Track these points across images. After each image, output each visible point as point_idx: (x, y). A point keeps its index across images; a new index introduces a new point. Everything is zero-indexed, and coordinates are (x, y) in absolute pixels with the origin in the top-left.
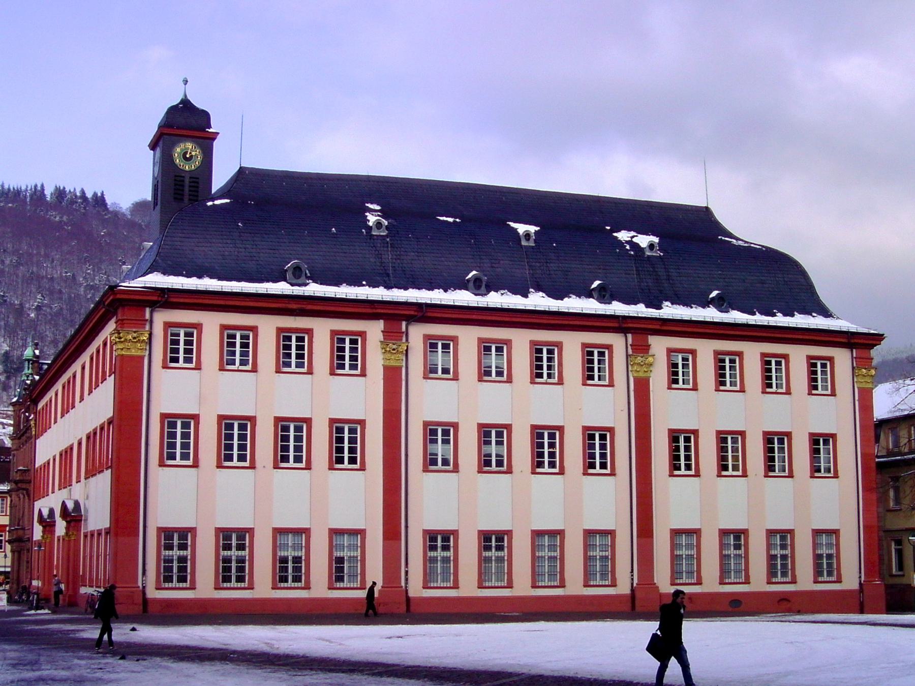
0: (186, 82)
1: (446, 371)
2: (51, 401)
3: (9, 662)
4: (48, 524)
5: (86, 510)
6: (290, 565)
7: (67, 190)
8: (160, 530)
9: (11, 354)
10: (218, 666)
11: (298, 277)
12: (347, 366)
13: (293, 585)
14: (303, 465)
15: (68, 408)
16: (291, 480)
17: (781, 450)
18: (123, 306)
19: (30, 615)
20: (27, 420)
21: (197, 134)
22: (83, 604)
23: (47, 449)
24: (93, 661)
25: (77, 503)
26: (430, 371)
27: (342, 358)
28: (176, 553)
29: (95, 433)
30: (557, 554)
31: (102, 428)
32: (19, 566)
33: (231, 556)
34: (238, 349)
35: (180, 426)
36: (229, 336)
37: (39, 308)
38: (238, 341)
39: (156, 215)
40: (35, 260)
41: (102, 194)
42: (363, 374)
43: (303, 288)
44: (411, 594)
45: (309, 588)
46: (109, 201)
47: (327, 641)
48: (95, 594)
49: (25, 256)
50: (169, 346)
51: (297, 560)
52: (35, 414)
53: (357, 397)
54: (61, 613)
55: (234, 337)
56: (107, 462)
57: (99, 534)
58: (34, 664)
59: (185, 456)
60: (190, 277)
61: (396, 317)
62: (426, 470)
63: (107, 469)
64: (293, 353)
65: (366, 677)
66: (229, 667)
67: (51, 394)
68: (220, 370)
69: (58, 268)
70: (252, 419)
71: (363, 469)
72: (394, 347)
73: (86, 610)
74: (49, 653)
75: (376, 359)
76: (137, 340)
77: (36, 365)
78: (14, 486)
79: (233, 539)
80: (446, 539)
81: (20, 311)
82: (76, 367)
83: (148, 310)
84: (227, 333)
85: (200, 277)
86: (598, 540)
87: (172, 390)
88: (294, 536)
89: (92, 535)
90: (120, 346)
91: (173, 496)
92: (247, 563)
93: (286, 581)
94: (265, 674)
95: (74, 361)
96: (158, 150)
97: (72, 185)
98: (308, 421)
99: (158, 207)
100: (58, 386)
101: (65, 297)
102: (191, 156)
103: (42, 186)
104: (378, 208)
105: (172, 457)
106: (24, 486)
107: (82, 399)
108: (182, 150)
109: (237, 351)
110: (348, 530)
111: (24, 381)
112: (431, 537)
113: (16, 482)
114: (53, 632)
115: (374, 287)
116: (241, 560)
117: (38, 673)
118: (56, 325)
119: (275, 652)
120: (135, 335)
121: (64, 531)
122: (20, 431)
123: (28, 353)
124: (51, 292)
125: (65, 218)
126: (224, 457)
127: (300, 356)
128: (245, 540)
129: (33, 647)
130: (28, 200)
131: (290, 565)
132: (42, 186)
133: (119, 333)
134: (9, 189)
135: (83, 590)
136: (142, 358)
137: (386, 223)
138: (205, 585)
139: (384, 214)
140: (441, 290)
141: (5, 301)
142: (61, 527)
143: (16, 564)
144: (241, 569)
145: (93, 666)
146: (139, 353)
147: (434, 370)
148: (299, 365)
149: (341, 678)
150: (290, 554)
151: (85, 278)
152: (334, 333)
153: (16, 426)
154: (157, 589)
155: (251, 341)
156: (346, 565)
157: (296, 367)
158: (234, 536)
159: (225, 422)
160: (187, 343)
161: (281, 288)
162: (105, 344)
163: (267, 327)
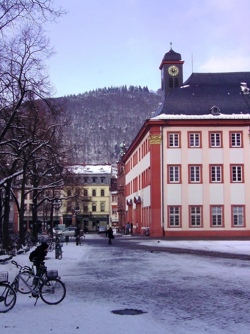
0: (171, 44)
2: (130, 161)
3: (113, 253)
4: (130, 205)
5: (143, 200)
6: (217, 218)
7: (134, 86)
8: (168, 206)
9: (118, 146)
10: (185, 255)
11: (216, 112)
13: (218, 226)
14: (221, 181)
15: (135, 164)
16: (216, 187)
18: (152, 126)
19: (124, 237)
20: (122, 169)
22: (142, 233)
23: (129, 178)
24: (141, 253)
25: (139, 198)
27: (172, 142)
28: (174, 215)
29: (145, 172)
31: (147, 171)
32: (121, 220)
33: (195, 215)
34: (194, 140)
35: (174, 170)
37: (126, 129)
38: (194, 137)
39: (163, 93)
40: (124, 112)
42: (242, 147)
43: (218, 116)
45: (224, 227)
46: (149, 89)
47: (228, 246)
48: (146, 229)
49: (121, 111)
50: (169, 140)
51: (219, 216)
52: (125, 166)
54: (134, 236)
55: (193, 135)
56: (149, 183)
57: (147, 208)
58: (120, 254)
60: (176, 115)
63: (149, 185)
64: (215, 140)
65: (239, 260)
66: (189, 256)
67: (129, 159)
68: (209, 148)
69: (133, 114)
70: (201, 165)
71: (243, 182)
73: (143, 235)
74: (127, 250)
76: (157, 139)
77: (124, 149)
78: (118, 192)
79: (196, 209)
81: (120, 130)
82: (137, 149)
84: (232, 134)
85: (179, 114)
89: (145, 209)
90: (152, 141)
91: (172, 194)
92: (201, 218)
93: (215, 224)
94: (202, 259)
95: (136, 147)
96: (163, 69)
97: (136, 84)
98: (222, 165)
99: (164, 90)
100: (132, 156)
101: (136, 124)
102: (175, 71)
103: (126, 86)
104: (246, 84)
106: (122, 192)
107: (140, 160)
108: (171, 69)
109: (194, 141)
110: (218, 205)
111: (120, 155)
113: (119, 191)
114: (131, 243)
115: (245, 114)
116: (177, 217)
117: (121, 257)
119: (208, 250)
120: (157, 137)
121: (135, 207)
122: (120, 172)
123: (122, 145)
124: (131, 123)
125: (134, 97)
126: (191, 179)
127: (218, 141)
128: (200, 209)
129: (122, 248)
130: (121, 91)
131: (217, 218)
132: (126, 86)
133: (151, 136)
134: (114, 88)
135: (142, 228)
136: (160, 145)
137: (249, 89)
138: (185, 226)
139: (248, 86)
141: (115, 127)
142: (134, 206)
143: (120, 219)
145: (141, 255)
146: (159, 143)
149: (230, 261)
150: (217, 214)
151: (142, 117)
152: (230, 132)
153: (119, 171)
154: (168, 227)
155: (199, 137)
156: (238, 218)
157: (217, 145)
160: (175, 138)
162: (146, 141)
163: (205, 131)
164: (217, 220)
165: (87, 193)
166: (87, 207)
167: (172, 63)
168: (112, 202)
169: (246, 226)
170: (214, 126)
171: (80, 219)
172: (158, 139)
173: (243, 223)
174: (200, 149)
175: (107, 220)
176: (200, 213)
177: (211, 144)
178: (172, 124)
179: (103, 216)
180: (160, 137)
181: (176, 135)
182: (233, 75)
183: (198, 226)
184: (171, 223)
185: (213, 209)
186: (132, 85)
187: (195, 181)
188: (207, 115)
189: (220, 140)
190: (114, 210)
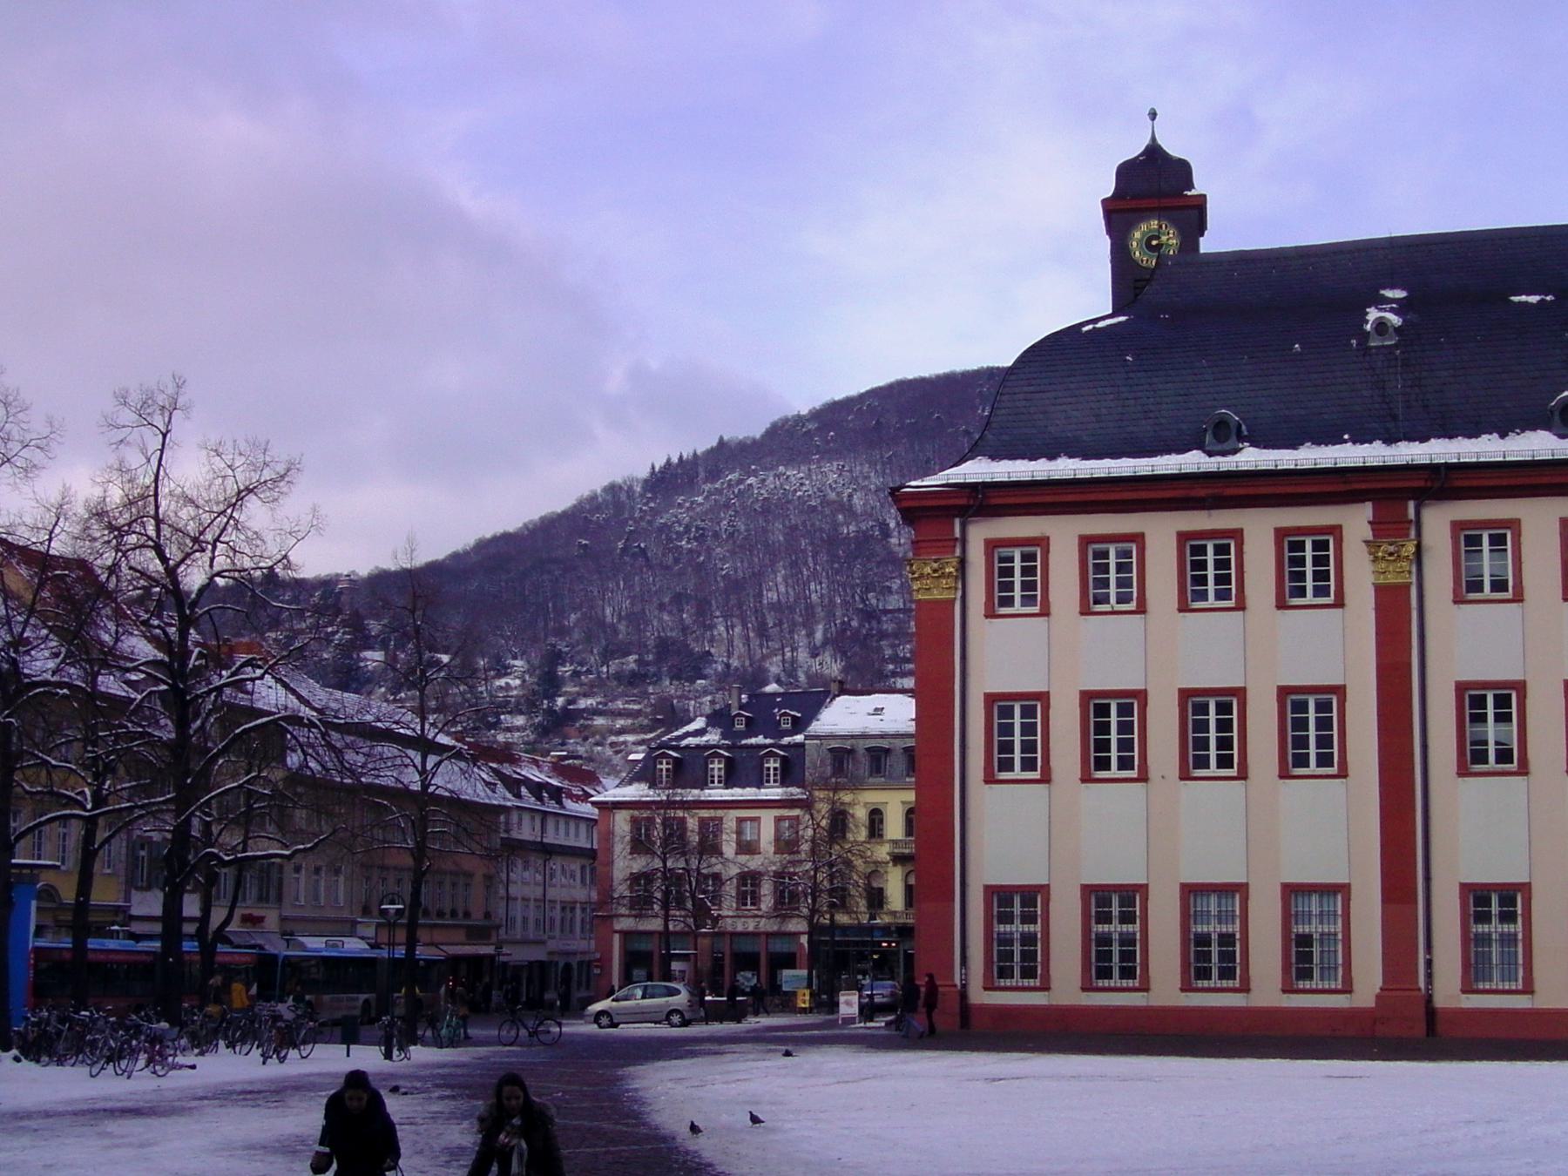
0: (1153, 115)
1: (1499, 585)
6: (1215, 949)
11: (1223, 437)
12: (1309, 591)
14: (1514, 766)
16: (1115, 802)
21: (1166, 202)
26: (1467, 588)
33: (1490, 934)
35: (1019, 715)
36: (1097, 555)
43: (1230, 458)
44: (1440, 1002)
51: (1226, 939)
53: (1332, 646)
55: (1105, 555)
59: (1125, 764)
60: (1477, 436)
61: (1395, 496)
62: (1463, 771)
64: (1208, 576)
70: (1141, 695)
72: (1391, 549)
75: (1360, 574)
83: (1411, 505)
84: (1288, 543)
85: (1052, 457)
87: (1004, 654)
88: (1321, 896)
105: (1007, 765)
108: (1143, 234)
109: (1109, 582)
112: (1477, 898)
120: (935, 565)
131: (1215, 949)
136: (1407, 587)
140: (1495, 435)
144: (1127, 956)
146: (946, 596)
147: (1476, 586)
148: (1221, 595)
150: (1213, 928)
156: (1316, 949)
158: (1115, 901)
159: (1291, 698)
161: (1193, 461)
163: (1161, 533)
164: (1215, 958)
166: (881, 890)
167: (1147, 209)
169: (1355, 987)
170: (1203, 508)
172: (943, 576)
173: (1340, 970)
174: (1514, 605)
176: (1515, 922)
177: (1190, 595)
178: (1470, 488)
180: (1411, 548)
181: (1219, 550)
182: (1350, 252)
183: (1125, 983)
184: (999, 971)
185: (1300, 905)
187: (1213, 770)
188: (995, 464)
189: (1332, 568)
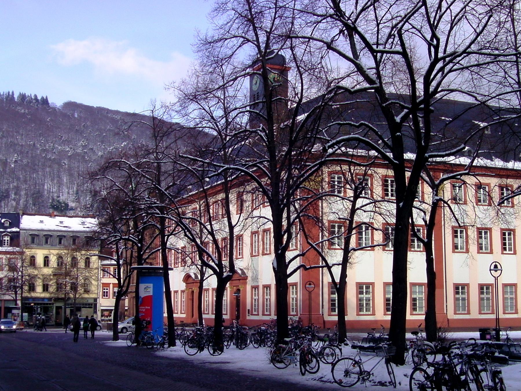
7: (27, 95)
17: (510, 239)
30: (514, 296)
37: (16, 162)
41: (47, 97)
44: (326, 319)
46: (50, 101)
80: (368, 288)
86: (417, 288)
97: (30, 91)
103: (13, 92)
112: (457, 287)
118: (26, 171)
124: (21, 153)
132: (13, 92)
165: (34, 260)
166: (34, 284)
168: (103, 277)
171: (50, 304)
175: (93, 306)
179: (88, 301)
186: (23, 91)
190: (106, 291)
